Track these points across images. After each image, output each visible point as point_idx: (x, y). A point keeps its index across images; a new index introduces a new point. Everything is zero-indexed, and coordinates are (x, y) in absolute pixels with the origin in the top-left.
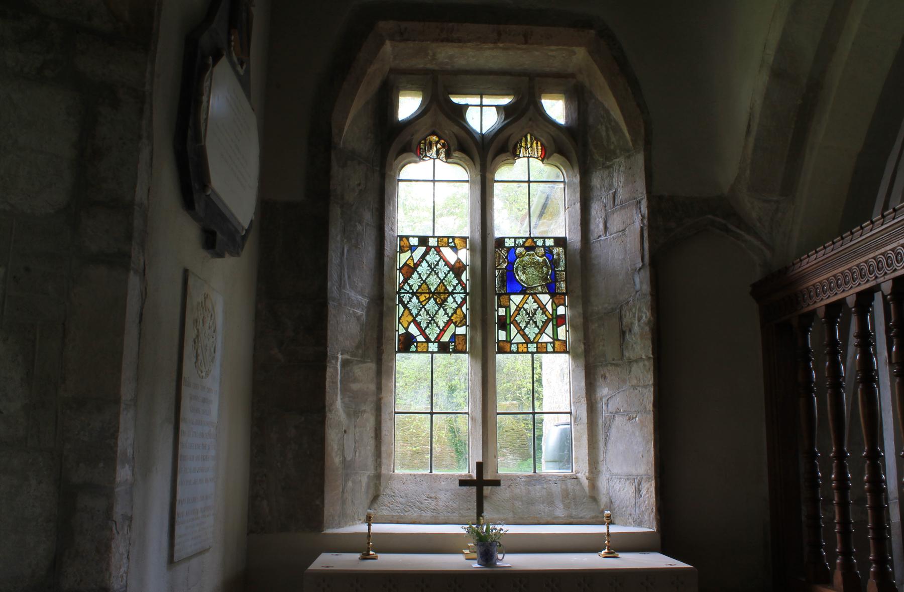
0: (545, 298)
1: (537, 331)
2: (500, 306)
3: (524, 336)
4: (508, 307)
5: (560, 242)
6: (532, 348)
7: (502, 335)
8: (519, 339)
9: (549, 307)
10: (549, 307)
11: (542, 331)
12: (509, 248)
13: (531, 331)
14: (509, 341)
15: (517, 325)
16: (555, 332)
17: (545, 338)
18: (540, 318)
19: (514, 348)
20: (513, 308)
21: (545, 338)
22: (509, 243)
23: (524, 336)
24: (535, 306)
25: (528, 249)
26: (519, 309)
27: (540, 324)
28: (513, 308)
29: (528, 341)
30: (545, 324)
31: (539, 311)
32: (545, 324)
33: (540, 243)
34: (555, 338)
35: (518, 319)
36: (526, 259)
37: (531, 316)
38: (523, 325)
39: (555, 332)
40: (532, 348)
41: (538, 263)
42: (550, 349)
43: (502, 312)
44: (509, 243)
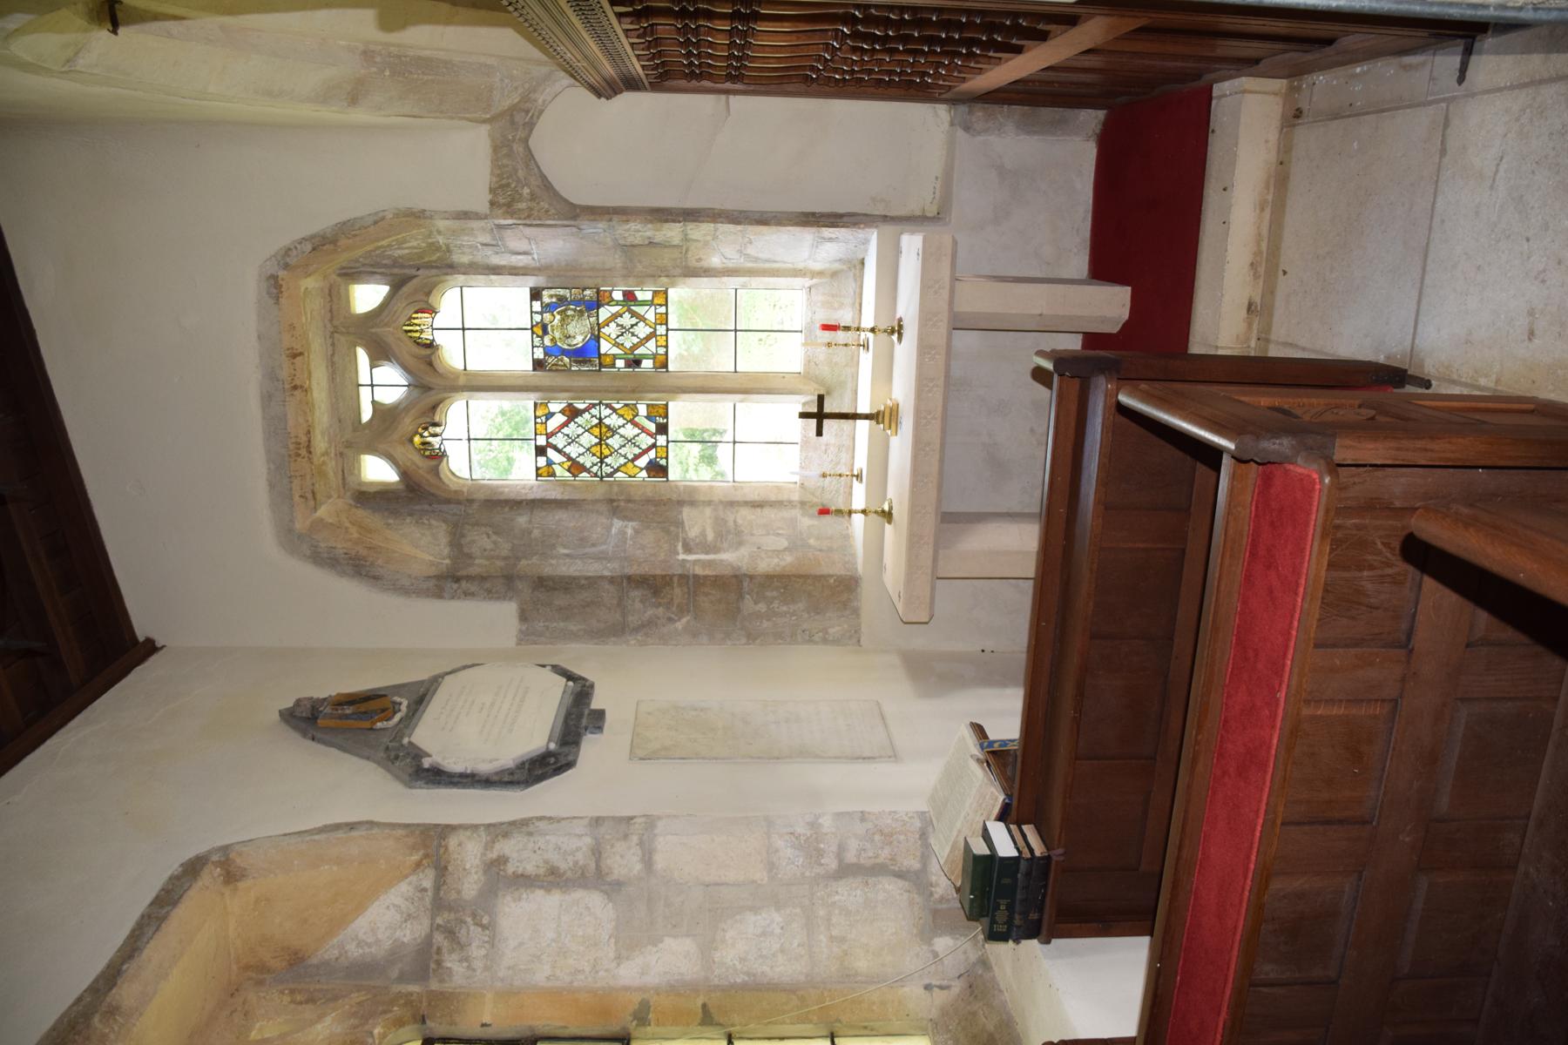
0: (605, 313)
1: (641, 324)
2: (613, 366)
3: (648, 338)
4: (615, 357)
5: (535, 295)
6: (661, 330)
7: (647, 364)
8: (651, 344)
9: (615, 309)
10: (615, 309)
11: (642, 318)
12: (546, 354)
13: (642, 330)
14: (654, 357)
15: (635, 347)
16: (643, 303)
17: (651, 316)
18: (627, 320)
19: (662, 351)
20: (616, 351)
21: (651, 316)
22: (539, 354)
23: (648, 338)
24: (613, 325)
25: (545, 332)
26: (617, 345)
27: (634, 320)
28: (616, 351)
29: (653, 335)
30: (634, 314)
31: (619, 320)
32: (634, 314)
33: (538, 318)
34: (651, 303)
35: (628, 345)
36: (557, 335)
37: (624, 331)
38: (635, 340)
39: (643, 303)
40: (661, 330)
41: (563, 320)
42: (663, 310)
43: (620, 363)
44: (539, 354)
